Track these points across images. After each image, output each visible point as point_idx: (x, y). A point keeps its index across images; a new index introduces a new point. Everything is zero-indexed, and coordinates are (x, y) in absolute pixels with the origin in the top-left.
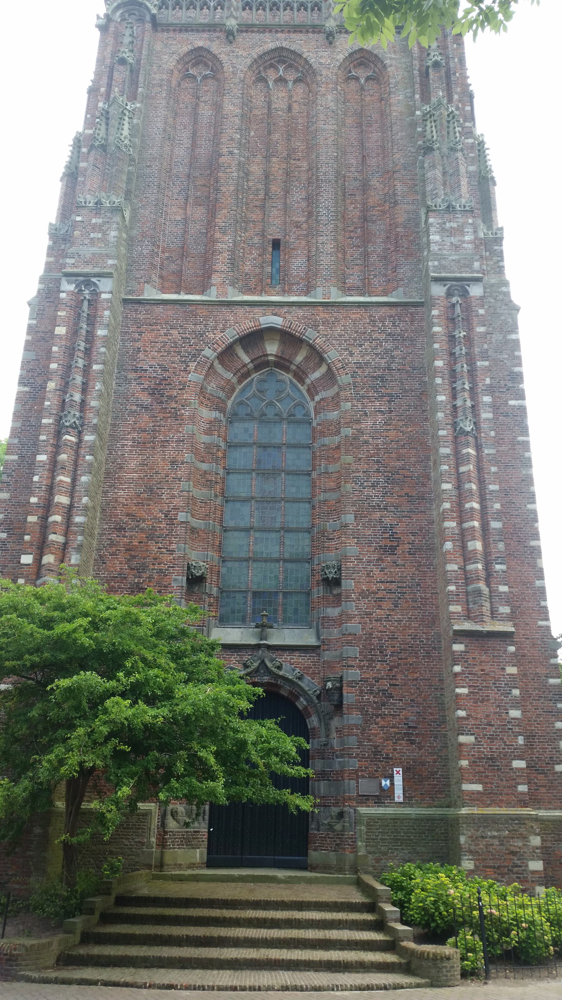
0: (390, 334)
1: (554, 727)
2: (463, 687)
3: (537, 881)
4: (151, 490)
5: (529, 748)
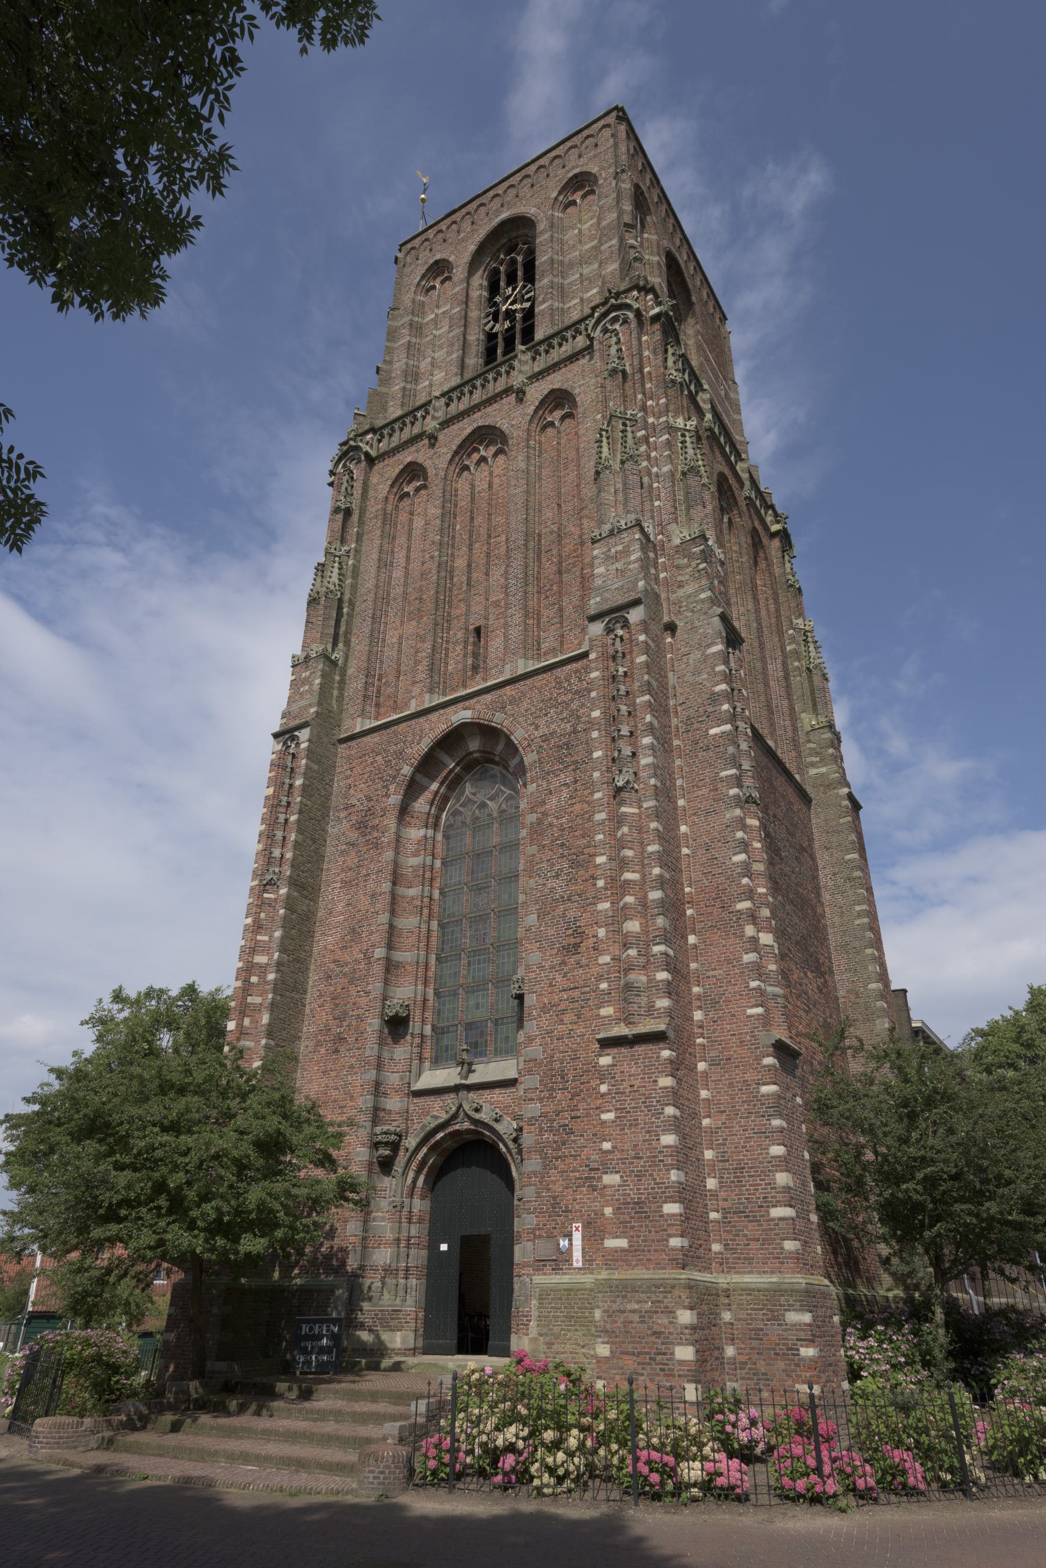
0: (576, 693)
1: (768, 1154)
2: (609, 1111)
3: (686, 1376)
4: (354, 930)
5: (736, 1186)
